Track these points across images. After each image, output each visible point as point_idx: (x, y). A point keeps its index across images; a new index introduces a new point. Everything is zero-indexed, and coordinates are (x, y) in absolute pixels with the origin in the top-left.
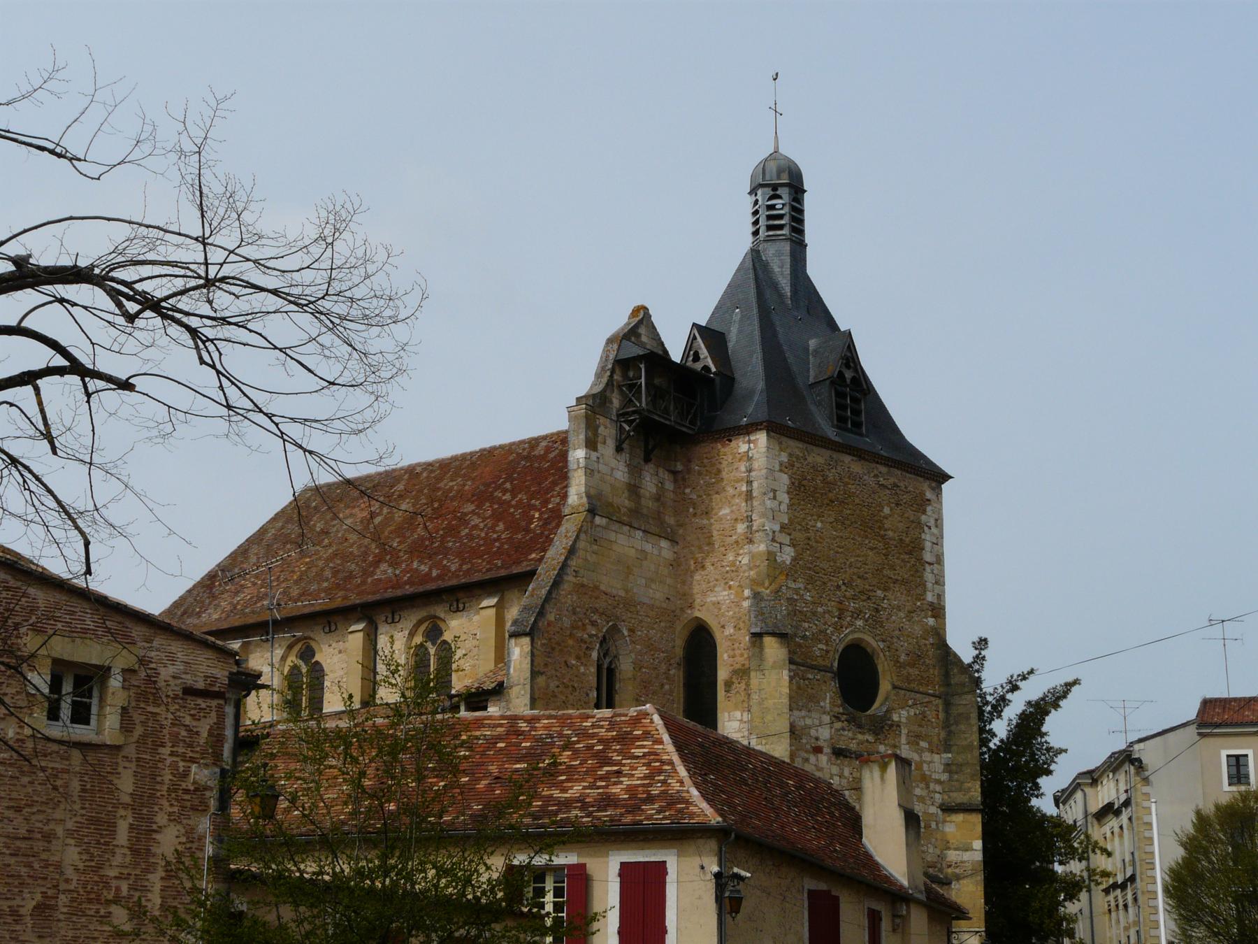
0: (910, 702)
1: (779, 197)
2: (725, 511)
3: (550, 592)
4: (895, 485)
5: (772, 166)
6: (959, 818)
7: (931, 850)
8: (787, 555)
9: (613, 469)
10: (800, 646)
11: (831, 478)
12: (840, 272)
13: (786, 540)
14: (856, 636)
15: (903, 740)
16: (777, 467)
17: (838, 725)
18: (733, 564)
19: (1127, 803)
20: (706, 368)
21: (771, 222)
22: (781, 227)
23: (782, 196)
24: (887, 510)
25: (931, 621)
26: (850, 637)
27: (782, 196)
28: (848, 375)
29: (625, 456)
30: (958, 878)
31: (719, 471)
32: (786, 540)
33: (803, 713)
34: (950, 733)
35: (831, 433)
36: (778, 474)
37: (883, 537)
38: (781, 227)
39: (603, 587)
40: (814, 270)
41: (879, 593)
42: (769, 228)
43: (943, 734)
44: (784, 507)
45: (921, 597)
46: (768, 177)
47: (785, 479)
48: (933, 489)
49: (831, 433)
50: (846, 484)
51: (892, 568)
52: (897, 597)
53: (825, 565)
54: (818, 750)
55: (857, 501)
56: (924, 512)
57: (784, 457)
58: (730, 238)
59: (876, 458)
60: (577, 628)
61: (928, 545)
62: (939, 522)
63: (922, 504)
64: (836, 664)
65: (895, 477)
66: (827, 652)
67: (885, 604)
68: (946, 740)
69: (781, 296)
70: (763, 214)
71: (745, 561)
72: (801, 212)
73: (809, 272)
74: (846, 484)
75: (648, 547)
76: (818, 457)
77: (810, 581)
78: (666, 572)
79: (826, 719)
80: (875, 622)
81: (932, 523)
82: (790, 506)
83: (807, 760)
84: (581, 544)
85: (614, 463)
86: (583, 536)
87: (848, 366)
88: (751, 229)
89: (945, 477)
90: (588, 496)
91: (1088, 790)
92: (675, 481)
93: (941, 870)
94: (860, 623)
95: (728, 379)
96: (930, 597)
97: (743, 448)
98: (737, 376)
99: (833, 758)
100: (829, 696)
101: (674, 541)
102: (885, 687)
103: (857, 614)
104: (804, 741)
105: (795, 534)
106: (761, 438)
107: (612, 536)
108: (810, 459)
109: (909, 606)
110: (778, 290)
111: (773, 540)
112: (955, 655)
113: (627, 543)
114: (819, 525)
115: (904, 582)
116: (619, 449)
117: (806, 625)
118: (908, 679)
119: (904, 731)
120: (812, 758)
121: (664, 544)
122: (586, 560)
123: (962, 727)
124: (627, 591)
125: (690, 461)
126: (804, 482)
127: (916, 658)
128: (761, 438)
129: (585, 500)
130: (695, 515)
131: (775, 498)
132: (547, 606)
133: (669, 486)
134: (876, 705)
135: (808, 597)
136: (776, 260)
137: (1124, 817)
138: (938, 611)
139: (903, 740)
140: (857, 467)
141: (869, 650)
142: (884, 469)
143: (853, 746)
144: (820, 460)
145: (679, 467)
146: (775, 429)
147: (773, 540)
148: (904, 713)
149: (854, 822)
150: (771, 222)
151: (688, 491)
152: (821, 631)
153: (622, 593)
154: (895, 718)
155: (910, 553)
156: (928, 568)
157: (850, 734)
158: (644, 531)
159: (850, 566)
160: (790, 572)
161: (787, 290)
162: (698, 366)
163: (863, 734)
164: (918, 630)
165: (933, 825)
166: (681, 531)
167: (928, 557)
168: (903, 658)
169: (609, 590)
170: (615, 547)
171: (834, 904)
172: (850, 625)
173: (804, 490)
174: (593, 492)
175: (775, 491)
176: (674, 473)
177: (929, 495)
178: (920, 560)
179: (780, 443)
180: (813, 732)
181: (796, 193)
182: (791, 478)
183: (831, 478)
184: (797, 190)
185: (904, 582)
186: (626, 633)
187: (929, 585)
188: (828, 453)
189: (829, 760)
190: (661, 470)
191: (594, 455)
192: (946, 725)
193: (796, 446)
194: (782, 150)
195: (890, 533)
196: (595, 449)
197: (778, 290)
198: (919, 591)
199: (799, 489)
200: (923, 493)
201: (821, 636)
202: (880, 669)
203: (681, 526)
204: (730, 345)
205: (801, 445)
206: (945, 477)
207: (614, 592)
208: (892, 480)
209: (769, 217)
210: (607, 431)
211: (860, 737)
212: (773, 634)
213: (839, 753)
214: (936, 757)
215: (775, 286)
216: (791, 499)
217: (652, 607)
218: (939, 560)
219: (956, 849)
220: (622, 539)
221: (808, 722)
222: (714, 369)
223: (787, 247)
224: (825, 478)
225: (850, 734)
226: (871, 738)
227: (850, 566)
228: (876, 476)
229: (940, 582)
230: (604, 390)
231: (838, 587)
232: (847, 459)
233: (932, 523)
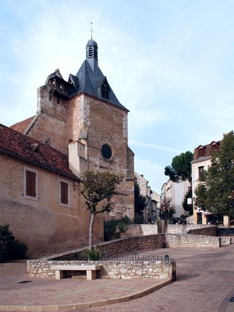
0: (119, 158)
1: (92, 49)
2: (76, 114)
3: (30, 129)
4: (116, 111)
5: (90, 42)
6: (130, 182)
7: (123, 189)
8: (89, 123)
9: (49, 104)
10: (92, 143)
11: (100, 108)
12: (106, 66)
13: (89, 120)
14: (106, 142)
15: (117, 165)
16: (87, 103)
17: (101, 161)
18: (77, 126)
19: (171, 187)
20: (73, 83)
21: (90, 54)
22: (92, 55)
23: (93, 50)
24: (114, 116)
25: (124, 141)
26: (104, 143)
27: (93, 50)
28: (105, 86)
29: (52, 101)
30: (129, 194)
31: (75, 105)
32: (89, 120)
33: (92, 158)
34: (128, 165)
35: (101, 98)
36: (87, 105)
37: (113, 122)
38: (92, 55)
39: (45, 129)
40: (100, 65)
41: (112, 134)
42: (89, 55)
43: (127, 165)
44: (88, 113)
45: (122, 136)
46: (89, 44)
47: (89, 106)
48: (125, 113)
49: (101, 98)
50: (104, 109)
51: (115, 129)
52: (116, 135)
53: (98, 126)
54: (96, 166)
55: (107, 113)
56: (123, 118)
57: (88, 101)
58: (82, 56)
59: (112, 104)
60: (38, 138)
61: (124, 125)
62: (127, 120)
63: (123, 116)
64: (101, 148)
65: (116, 109)
66: (99, 145)
67: (113, 136)
68: (127, 166)
69: (92, 70)
70: (88, 52)
71: (79, 124)
72: (97, 52)
73: (98, 66)
74: (104, 109)
75: (58, 122)
76: (97, 102)
77: (95, 129)
78: (63, 128)
79: (98, 159)
80: (111, 140)
81: (125, 120)
82: (90, 112)
83: (93, 168)
84: (39, 119)
85: (49, 102)
86: (39, 117)
87: (105, 84)
88: (86, 57)
89: (128, 111)
90: (41, 108)
91: (165, 186)
92: (66, 109)
93: (125, 193)
94: (107, 140)
95: (78, 86)
96: (124, 136)
97: (79, 99)
98: (80, 85)
99: (100, 168)
100: (99, 154)
101: (65, 122)
102: (113, 154)
103: (107, 138)
104: (92, 164)
105: (91, 119)
106: (83, 96)
107: (48, 119)
108: (95, 103)
109: (119, 138)
110: (91, 69)
111: (85, 119)
112: (129, 148)
113: (52, 121)
114: (97, 117)
115: (118, 132)
116: (50, 99)
117: (94, 139)
118: (119, 153)
119: (117, 164)
120: (95, 168)
121: (63, 122)
122: (41, 123)
123: (130, 163)
124: (52, 131)
125: (69, 104)
126: (94, 108)
127: (121, 149)
128: (83, 96)
129: (40, 109)
130: (70, 116)
131: (86, 110)
132: (29, 132)
133: (64, 110)
134: (111, 158)
135: (94, 133)
136: (91, 63)
137: (171, 189)
138: (126, 139)
139: (117, 165)
140: (107, 106)
141: (109, 146)
142: (114, 107)
143: (105, 166)
144: (98, 103)
145: (67, 106)
146: (86, 95)
147: (85, 119)
148: (117, 160)
149: (66, 158)
150: (90, 54)
151: (68, 111)
152: (97, 141)
153: (51, 132)
154: (115, 161)
155: (120, 126)
156: (124, 130)
157: (104, 163)
158: (57, 119)
159: (105, 127)
160: (90, 127)
161: (93, 69)
162: (71, 83)
163: (108, 163)
164: (121, 143)
165: (124, 184)
166: (67, 120)
167: (124, 127)
168: (117, 148)
169: (47, 130)
170: (49, 121)
171: (67, 185)
172: (105, 140)
173: (93, 109)
174: (43, 108)
175: (86, 109)
176: (66, 107)
177: (124, 114)
178: (122, 128)
179: (87, 98)
180: (95, 162)
181: (96, 48)
182: (90, 106)
183: (100, 108)
184: (96, 47)
185: (118, 132)
186: (52, 140)
187: (124, 134)
188: (100, 102)
189: (99, 169)
190: (62, 106)
191: (43, 100)
192: (128, 163)
193: (92, 100)
194: (93, 39)
195: (115, 121)
196: (43, 98)
197: (91, 69)
198: (122, 134)
199: (92, 109)
200: (123, 114)
201: (98, 142)
202: (112, 151)
203: (67, 119)
204: (79, 80)
205: (93, 99)
206: (128, 111)
207: (49, 131)
208: (115, 110)
209: (89, 51)
210: (47, 94)
211: (107, 164)
212: (84, 139)
213: (101, 167)
214: (125, 170)
215: (90, 68)
216: (90, 111)
217: (60, 136)
218: (127, 128)
219: (129, 188)
220: (51, 119)
221: (94, 160)
222: (74, 83)
223: (93, 59)
224: (99, 107)
225: (104, 163)
226: (109, 165)
227: (105, 127)
228: (112, 109)
229: (127, 133)
230: (46, 85)
231: (102, 132)
232: (105, 104)
233: (125, 120)
